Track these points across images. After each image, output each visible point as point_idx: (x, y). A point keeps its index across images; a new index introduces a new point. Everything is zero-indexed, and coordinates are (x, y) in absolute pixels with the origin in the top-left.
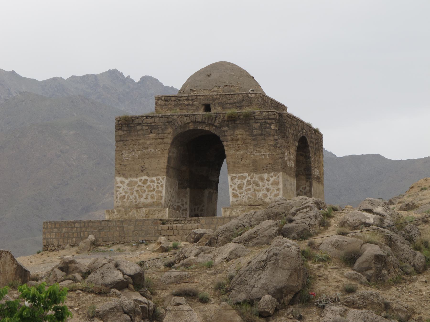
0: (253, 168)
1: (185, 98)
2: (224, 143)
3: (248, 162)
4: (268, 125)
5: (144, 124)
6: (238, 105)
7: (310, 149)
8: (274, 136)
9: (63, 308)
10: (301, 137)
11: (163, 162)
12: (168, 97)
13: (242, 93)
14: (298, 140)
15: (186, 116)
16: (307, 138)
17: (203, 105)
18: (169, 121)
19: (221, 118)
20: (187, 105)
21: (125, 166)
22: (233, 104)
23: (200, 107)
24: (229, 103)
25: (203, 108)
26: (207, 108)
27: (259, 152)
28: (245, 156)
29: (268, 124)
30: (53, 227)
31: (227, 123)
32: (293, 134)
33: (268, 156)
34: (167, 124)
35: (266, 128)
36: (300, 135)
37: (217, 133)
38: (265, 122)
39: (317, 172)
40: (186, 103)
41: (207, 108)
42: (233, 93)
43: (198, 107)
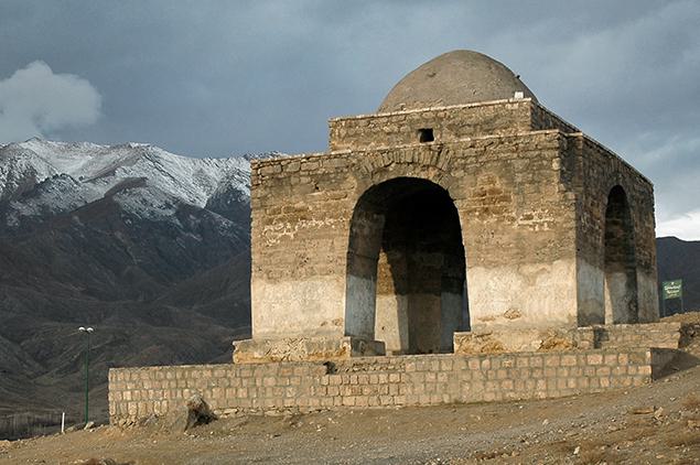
0: (516, 251)
1: (385, 120)
3: (506, 238)
5: (302, 173)
8: (611, 369)
10: (614, 188)
11: (342, 244)
12: (644, 179)
13: (494, 102)
14: (607, 193)
15: (382, 152)
16: (626, 190)
17: (420, 130)
18: (351, 165)
19: (451, 153)
20: (388, 134)
21: (271, 255)
22: (475, 125)
23: (413, 134)
24: (469, 125)
25: (419, 136)
26: (427, 135)
27: (529, 217)
29: (545, 159)
30: (128, 379)
32: (597, 180)
33: (546, 224)
35: (541, 167)
36: (612, 184)
37: (442, 183)
39: (644, 255)
40: (386, 129)
41: (427, 135)
42: (476, 104)
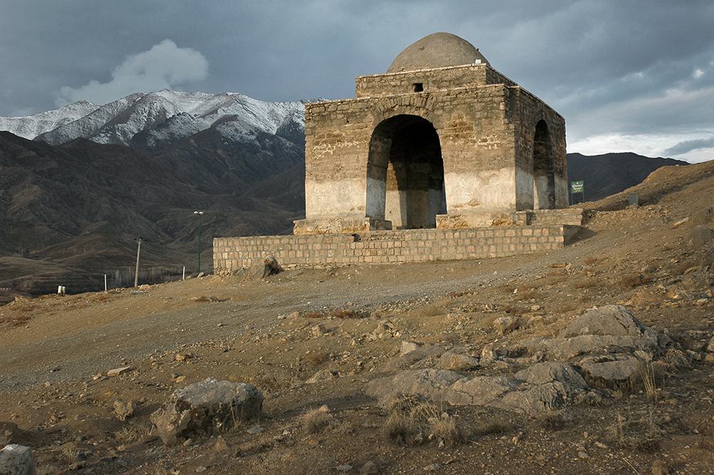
0: (476, 162)
2: (438, 132)
3: (469, 154)
4: (495, 105)
6: (457, 82)
7: (551, 136)
9: (122, 282)
11: (364, 157)
17: (414, 84)
18: (370, 107)
20: (394, 86)
21: (318, 165)
23: (410, 87)
24: (446, 81)
25: (414, 87)
27: (485, 141)
28: (634, 439)
31: (442, 104)
33: (495, 145)
34: (366, 110)
35: (492, 108)
36: (538, 119)
38: (491, 100)
40: (393, 83)
41: (419, 87)
43: (407, 88)
